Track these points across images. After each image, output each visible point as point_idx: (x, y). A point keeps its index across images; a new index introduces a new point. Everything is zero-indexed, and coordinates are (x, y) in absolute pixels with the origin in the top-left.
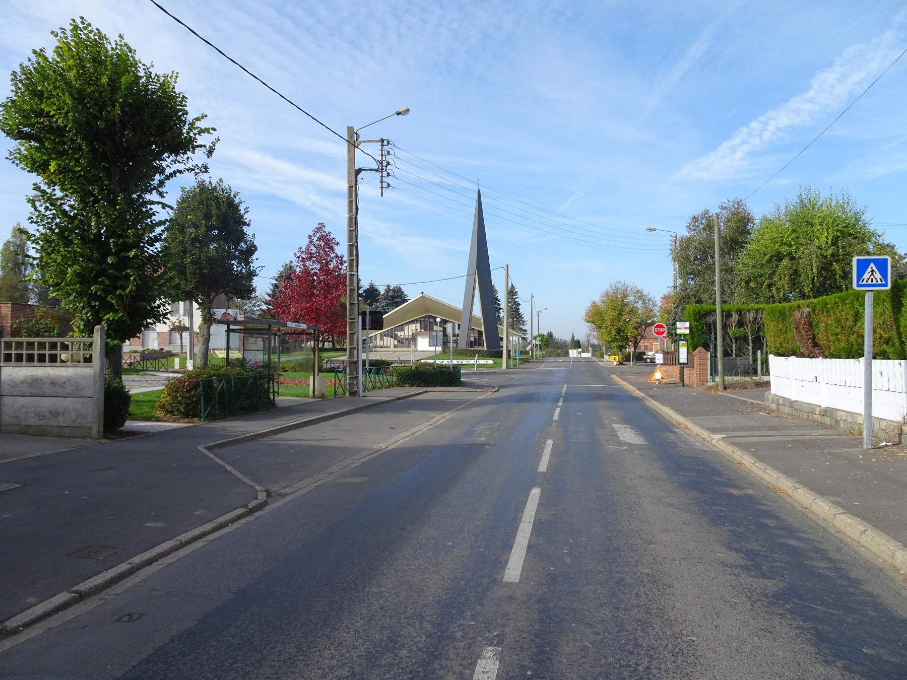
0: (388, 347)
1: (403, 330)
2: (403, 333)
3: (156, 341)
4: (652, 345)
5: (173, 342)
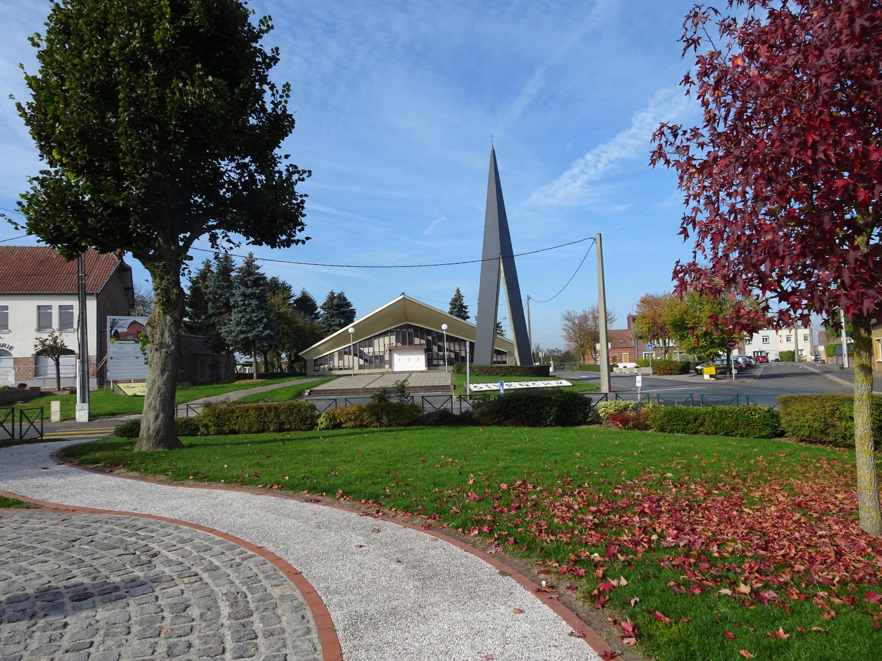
0: (350, 369)
1: (371, 345)
2: (371, 349)
3: (13, 372)
4: (621, 355)
5: (42, 372)
